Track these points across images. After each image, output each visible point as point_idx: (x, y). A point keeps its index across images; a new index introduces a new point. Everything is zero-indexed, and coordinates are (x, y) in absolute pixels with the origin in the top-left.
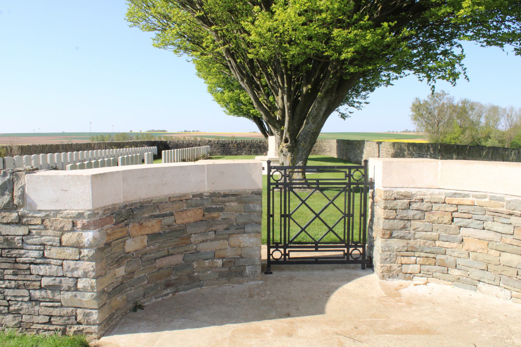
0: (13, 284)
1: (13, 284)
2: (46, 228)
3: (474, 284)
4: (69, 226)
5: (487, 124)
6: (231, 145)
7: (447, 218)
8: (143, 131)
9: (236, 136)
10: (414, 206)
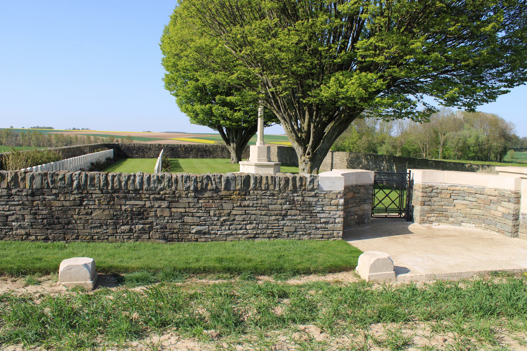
0: (309, 221)
1: (309, 221)
2: (325, 198)
3: (460, 223)
4: (335, 197)
5: (382, 131)
6: (180, 149)
7: (448, 196)
8: (26, 128)
9: (132, 135)
10: (434, 191)
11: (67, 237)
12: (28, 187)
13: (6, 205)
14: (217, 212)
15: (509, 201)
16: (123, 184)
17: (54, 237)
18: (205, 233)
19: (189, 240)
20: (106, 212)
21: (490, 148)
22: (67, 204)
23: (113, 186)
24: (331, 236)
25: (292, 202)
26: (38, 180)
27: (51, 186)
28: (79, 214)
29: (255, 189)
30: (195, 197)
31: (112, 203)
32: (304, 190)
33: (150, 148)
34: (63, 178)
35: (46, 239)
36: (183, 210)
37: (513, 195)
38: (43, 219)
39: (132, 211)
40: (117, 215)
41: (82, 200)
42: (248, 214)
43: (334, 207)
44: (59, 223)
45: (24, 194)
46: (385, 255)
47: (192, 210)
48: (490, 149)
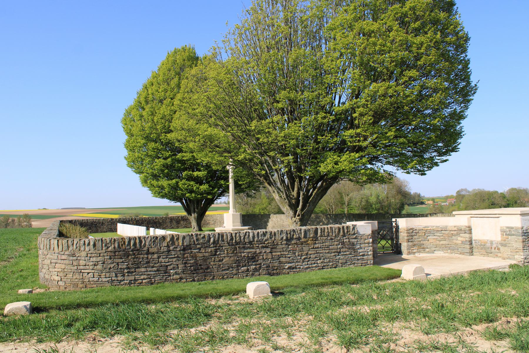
3: (433, 252)
7: (424, 234)
9: (30, 213)
11: (207, 278)
12: (180, 244)
13: (166, 258)
14: (300, 253)
15: (465, 233)
16: (242, 238)
17: (198, 279)
18: (293, 268)
19: (284, 274)
20: (232, 259)
21: (390, 205)
22: (207, 254)
23: (236, 240)
24: (366, 264)
25: (343, 243)
26: (187, 239)
27: (196, 243)
28: (214, 261)
29: (321, 236)
30: (286, 244)
31: (235, 252)
32: (349, 234)
33: (103, 223)
34: (204, 237)
35: (194, 280)
36: (279, 253)
37: (468, 229)
38: (191, 266)
39: (248, 256)
40: (239, 260)
41: (216, 251)
42: (318, 253)
43: (367, 245)
44: (202, 269)
45: (178, 249)
46: (420, 265)
47: (285, 253)
48: (390, 206)
